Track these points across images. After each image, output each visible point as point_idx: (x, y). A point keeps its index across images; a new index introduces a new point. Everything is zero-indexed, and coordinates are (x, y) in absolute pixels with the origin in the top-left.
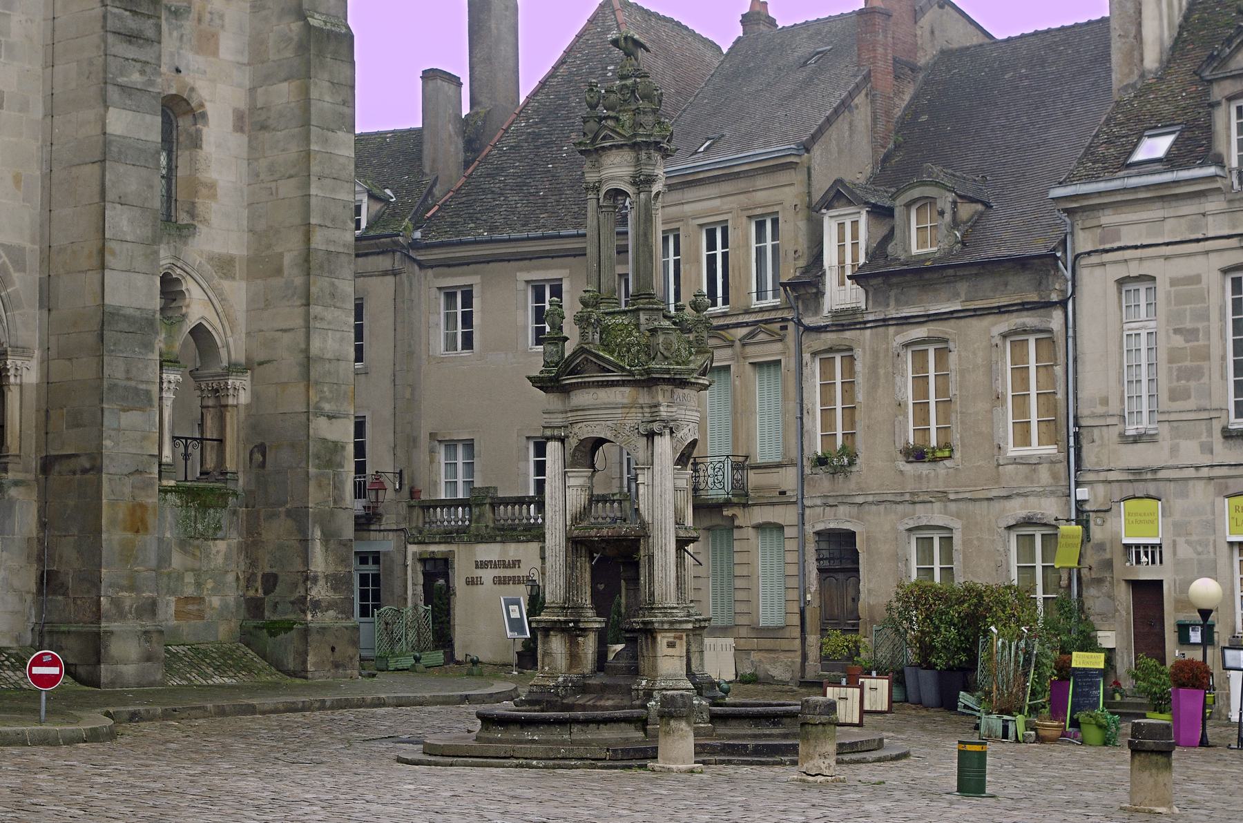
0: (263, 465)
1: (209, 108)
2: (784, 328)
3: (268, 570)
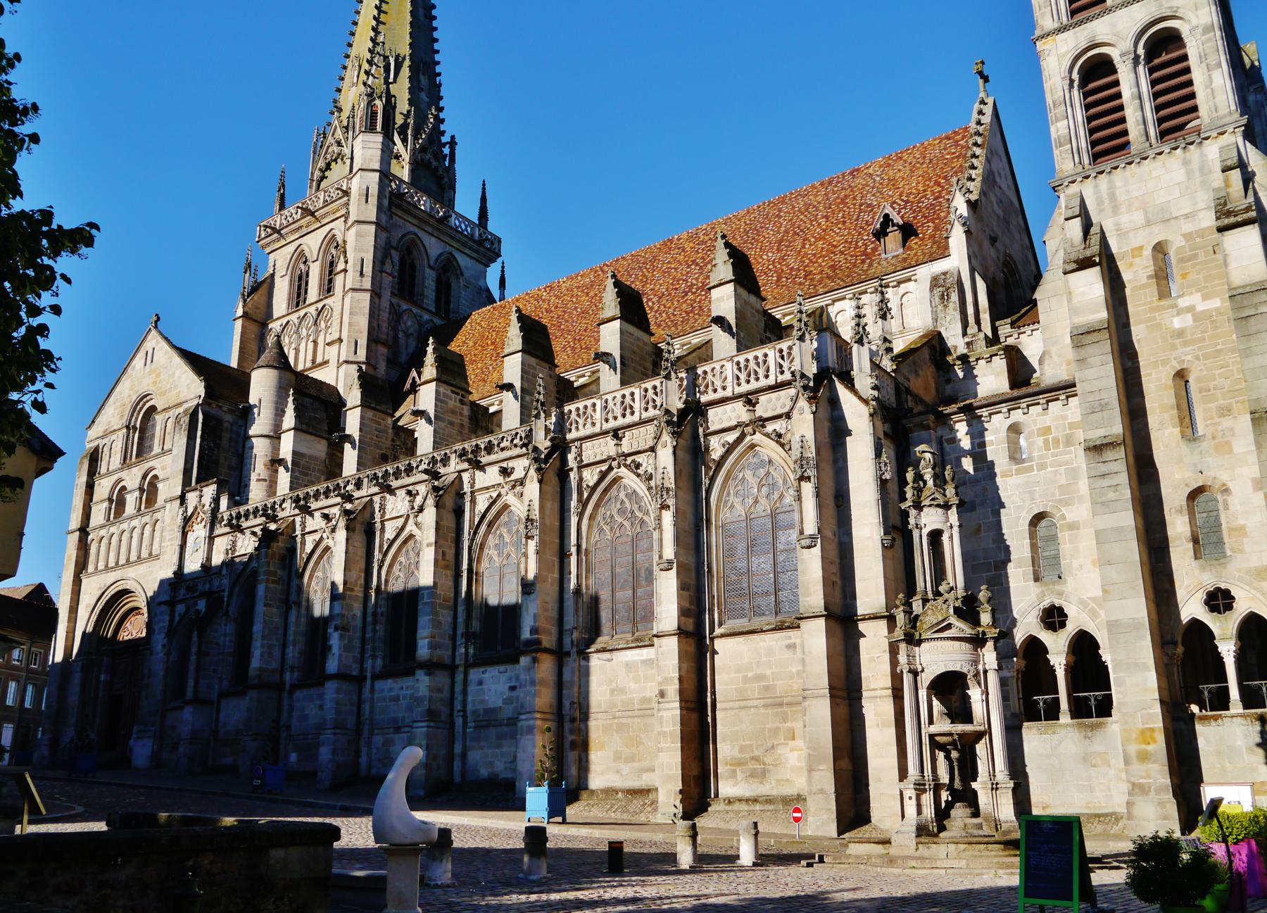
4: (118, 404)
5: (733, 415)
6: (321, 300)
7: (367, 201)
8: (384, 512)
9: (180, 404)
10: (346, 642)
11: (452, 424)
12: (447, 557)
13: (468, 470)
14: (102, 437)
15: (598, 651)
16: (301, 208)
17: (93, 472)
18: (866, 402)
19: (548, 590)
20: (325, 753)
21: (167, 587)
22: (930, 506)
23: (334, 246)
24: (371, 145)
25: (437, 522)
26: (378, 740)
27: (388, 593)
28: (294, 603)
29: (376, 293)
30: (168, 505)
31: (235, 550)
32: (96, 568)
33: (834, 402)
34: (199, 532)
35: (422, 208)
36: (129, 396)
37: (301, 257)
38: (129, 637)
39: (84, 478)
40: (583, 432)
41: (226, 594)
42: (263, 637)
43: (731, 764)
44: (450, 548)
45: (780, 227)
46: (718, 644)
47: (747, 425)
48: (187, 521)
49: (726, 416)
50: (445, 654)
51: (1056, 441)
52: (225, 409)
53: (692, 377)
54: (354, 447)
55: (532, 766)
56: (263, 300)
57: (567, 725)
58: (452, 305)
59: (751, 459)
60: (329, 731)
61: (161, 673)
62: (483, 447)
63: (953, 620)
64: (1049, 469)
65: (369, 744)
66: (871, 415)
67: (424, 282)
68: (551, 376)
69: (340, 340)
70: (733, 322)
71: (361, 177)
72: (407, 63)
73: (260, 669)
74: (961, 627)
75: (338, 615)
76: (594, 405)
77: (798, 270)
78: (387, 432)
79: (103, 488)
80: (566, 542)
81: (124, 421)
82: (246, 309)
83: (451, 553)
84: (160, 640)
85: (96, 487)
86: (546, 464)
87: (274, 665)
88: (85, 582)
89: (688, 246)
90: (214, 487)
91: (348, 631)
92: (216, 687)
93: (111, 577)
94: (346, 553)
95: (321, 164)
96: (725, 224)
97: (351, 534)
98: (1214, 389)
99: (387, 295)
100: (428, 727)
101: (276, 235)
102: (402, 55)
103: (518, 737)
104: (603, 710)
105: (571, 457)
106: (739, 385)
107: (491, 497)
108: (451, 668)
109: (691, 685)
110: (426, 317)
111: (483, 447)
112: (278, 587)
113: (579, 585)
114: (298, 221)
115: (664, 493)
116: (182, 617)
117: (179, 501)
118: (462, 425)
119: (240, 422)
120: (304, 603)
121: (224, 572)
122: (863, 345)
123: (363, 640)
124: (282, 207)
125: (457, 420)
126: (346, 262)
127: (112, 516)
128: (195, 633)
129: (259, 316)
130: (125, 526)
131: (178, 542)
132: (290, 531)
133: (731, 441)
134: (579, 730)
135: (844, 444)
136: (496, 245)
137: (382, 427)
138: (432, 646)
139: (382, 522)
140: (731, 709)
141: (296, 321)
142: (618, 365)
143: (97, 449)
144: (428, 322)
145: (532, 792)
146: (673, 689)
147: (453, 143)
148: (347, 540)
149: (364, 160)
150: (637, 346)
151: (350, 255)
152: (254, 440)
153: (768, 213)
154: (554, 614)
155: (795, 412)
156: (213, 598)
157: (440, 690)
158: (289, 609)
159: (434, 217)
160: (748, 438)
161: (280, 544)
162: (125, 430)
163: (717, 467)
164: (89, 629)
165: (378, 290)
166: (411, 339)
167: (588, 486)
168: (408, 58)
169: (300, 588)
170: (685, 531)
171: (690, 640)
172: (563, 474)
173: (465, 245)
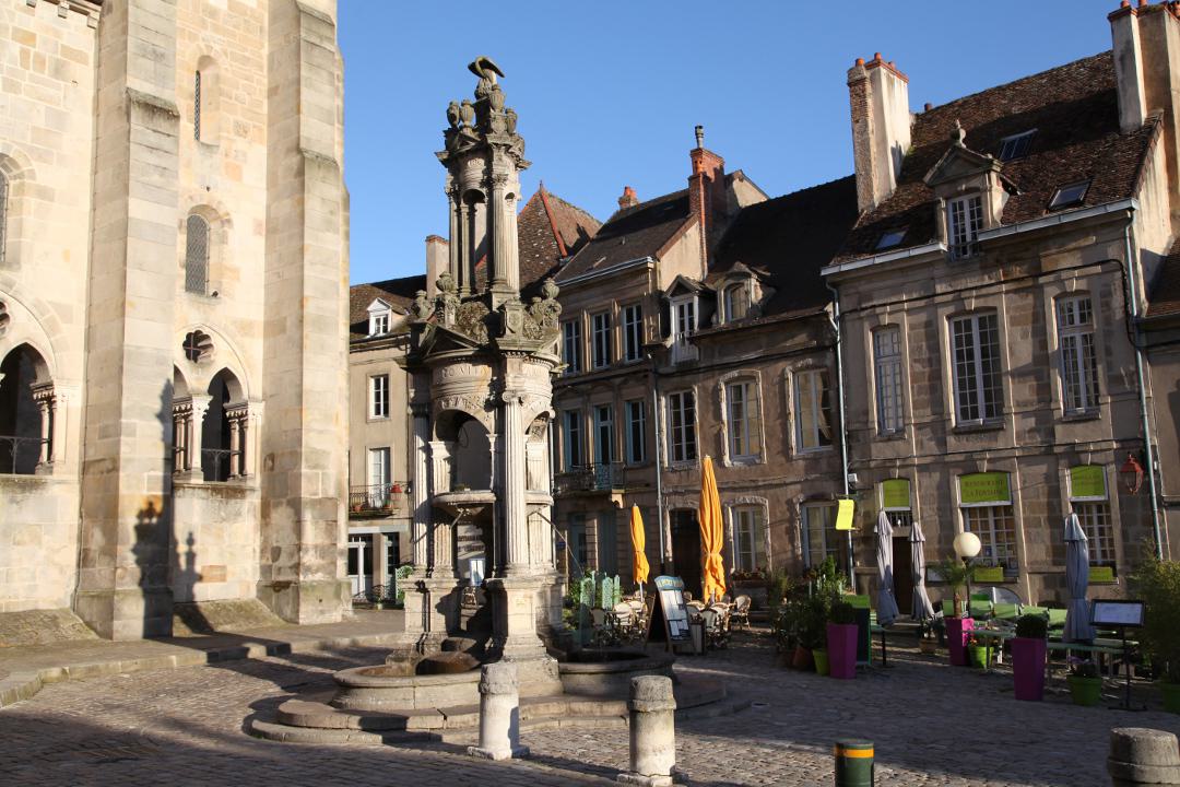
0: (272, 469)
1: (234, 217)
2: (646, 376)
3: (275, 545)
51: (40, 62)
64: (22, 96)
98: (236, 99)
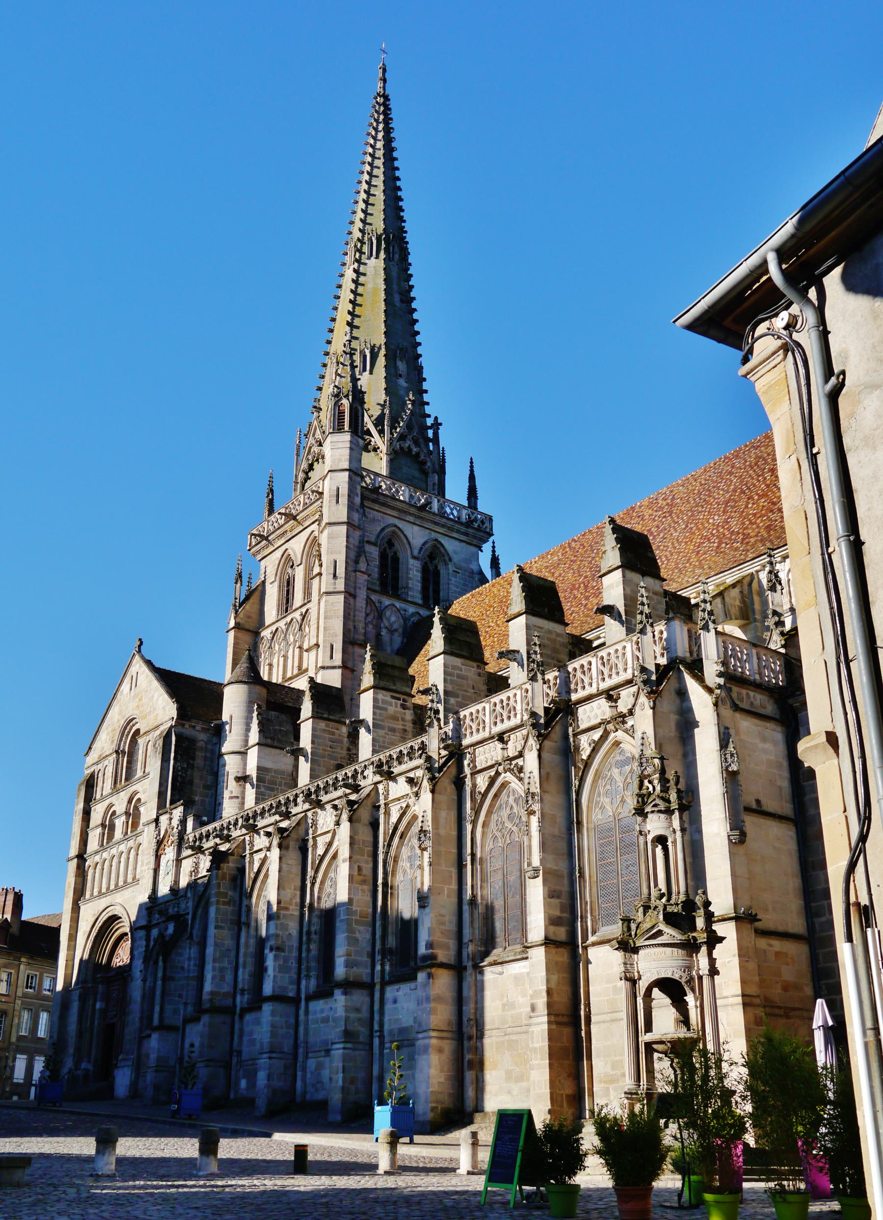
4: (110, 729)
5: (599, 712)
6: (305, 604)
7: (338, 502)
8: (316, 828)
9: (157, 727)
10: (281, 962)
11: (393, 730)
12: (364, 872)
13: (381, 782)
14: (97, 763)
15: (491, 965)
16: (285, 514)
17: (89, 799)
18: (710, 690)
19: (445, 903)
20: (262, 1076)
21: (145, 912)
22: (653, 812)
23: (313, 545)
24: (340, 445)
25: (351, 837)
26: (312, 1063)
27: (321, 910)
28: (244, 924)
29: (350, 594)
30: (146, 829)
31: (198, 872)
32: (92, 894)
33: (682, 693)
34: (170, 853)
35: (402, 498)
36: (118, 721)
37: (288, 562)
38: (121, 964)
39: (81, 806)
40: (476, 738)
41: (190, 917)
42: (214, 961)
43: (604, 1082)
44: (367, 862)
45: (730, 485)
46: (592, 953)
47: (609, 722)
48: (160, 843)
49: (593, 713)
50: (363, 973)
52: (198, 728)
53: (564, 675)
54: (307, 761)
55: (428, 1088)
56: (256, 607)
57: (466, 1043)
58: (441, 594)
59: (617, 757)
60: (265, 1055)
61: (139, 999)
62: (395, 757)
63: (662, 927)
65: (304, 1069)
66: (716, 704)
67: (408, 573)
68: (479, 675)
69: (317, 645)
70: (622, 610)
71: (331, 478)
72: (383, 352)
73: (212, 993)
74: (670, 934)
75: (273, 935)
76: (484, 709)
77: (738, 533)
78: (341, 742)
79: (97, 813)
80: (463, 851)
81: (114, 747)
82: (238, 620)
83: (367, 868)
84: (139, 964)
85: (92, 814)
86: (439, 773)
87: (226, 988)
88: (83, 908)
89: (647, 513)
90: (181, 809)
91: (283, 951)
92: (182, 1012)
93: (103, 902)
94: (279, 871)
95: (304, 465)
96: (683, 486)
97: (284, 852)
99: (362, 594)
100: (344, 1048)
101: (264, 542)
102: (378, 345)
103: (416, 1057)
104: (496, 1026)
105: (466, 762)
106: (604, 679)
107: (401, 807)
108: (369, 987)
109: (563, 998)
110: (411, 609)
111: (395, 757)
112: (230, 908)
113: (474, 896)
114: (282, 526)
115: (530, 798)
116: (156, 941)
117: (154, 824)
118: (405, 730)
119: (215, 740)
120: (253, 924)
121: (189, 895)
122: (708, 631)
123: (299, 960)
124: (271, 511)
125: (399, 726)
126: (321, 565)
127: (105, 841)
128: (161, 958)
129: (251, 625)
130: (114, 851)
131: (152, 866)
132: (241, 850)
133: (596, 739)
134: (476, 1048)
135: (692, 737)
136: (487, 524)
137: (337, 737)
138: (348, 965)
139: (314, 838)
140: (604, 1022)
141: (284, 627)
142: (525, 662)
143: (92, 776)
144: (413, 614)
145: (379, 1111)
146: (542, 1001)
147: (437, 425)
148: (280, 858)
149: (333, 461)
150: (548, 639)
151: (324, 558)
152: (226, 757)
153: (723, 469)
154: (453, 927)
155: (637, 708)
156: (179, 919)
157: (358, 1010)
158: (240, 930)
159: (415, 506)
160: (612, 735)
161: (230, 866)
162: (115, 755)
163: (585, 767)
164: (86, 956)
165: (352, 591)
166: (396, 634)
167: (480, 793)
168: (383, 347)
169: (249, 908)
170: (554, 836)
171: (561, 950)
172: (459, 783)
173: (451, 529)
